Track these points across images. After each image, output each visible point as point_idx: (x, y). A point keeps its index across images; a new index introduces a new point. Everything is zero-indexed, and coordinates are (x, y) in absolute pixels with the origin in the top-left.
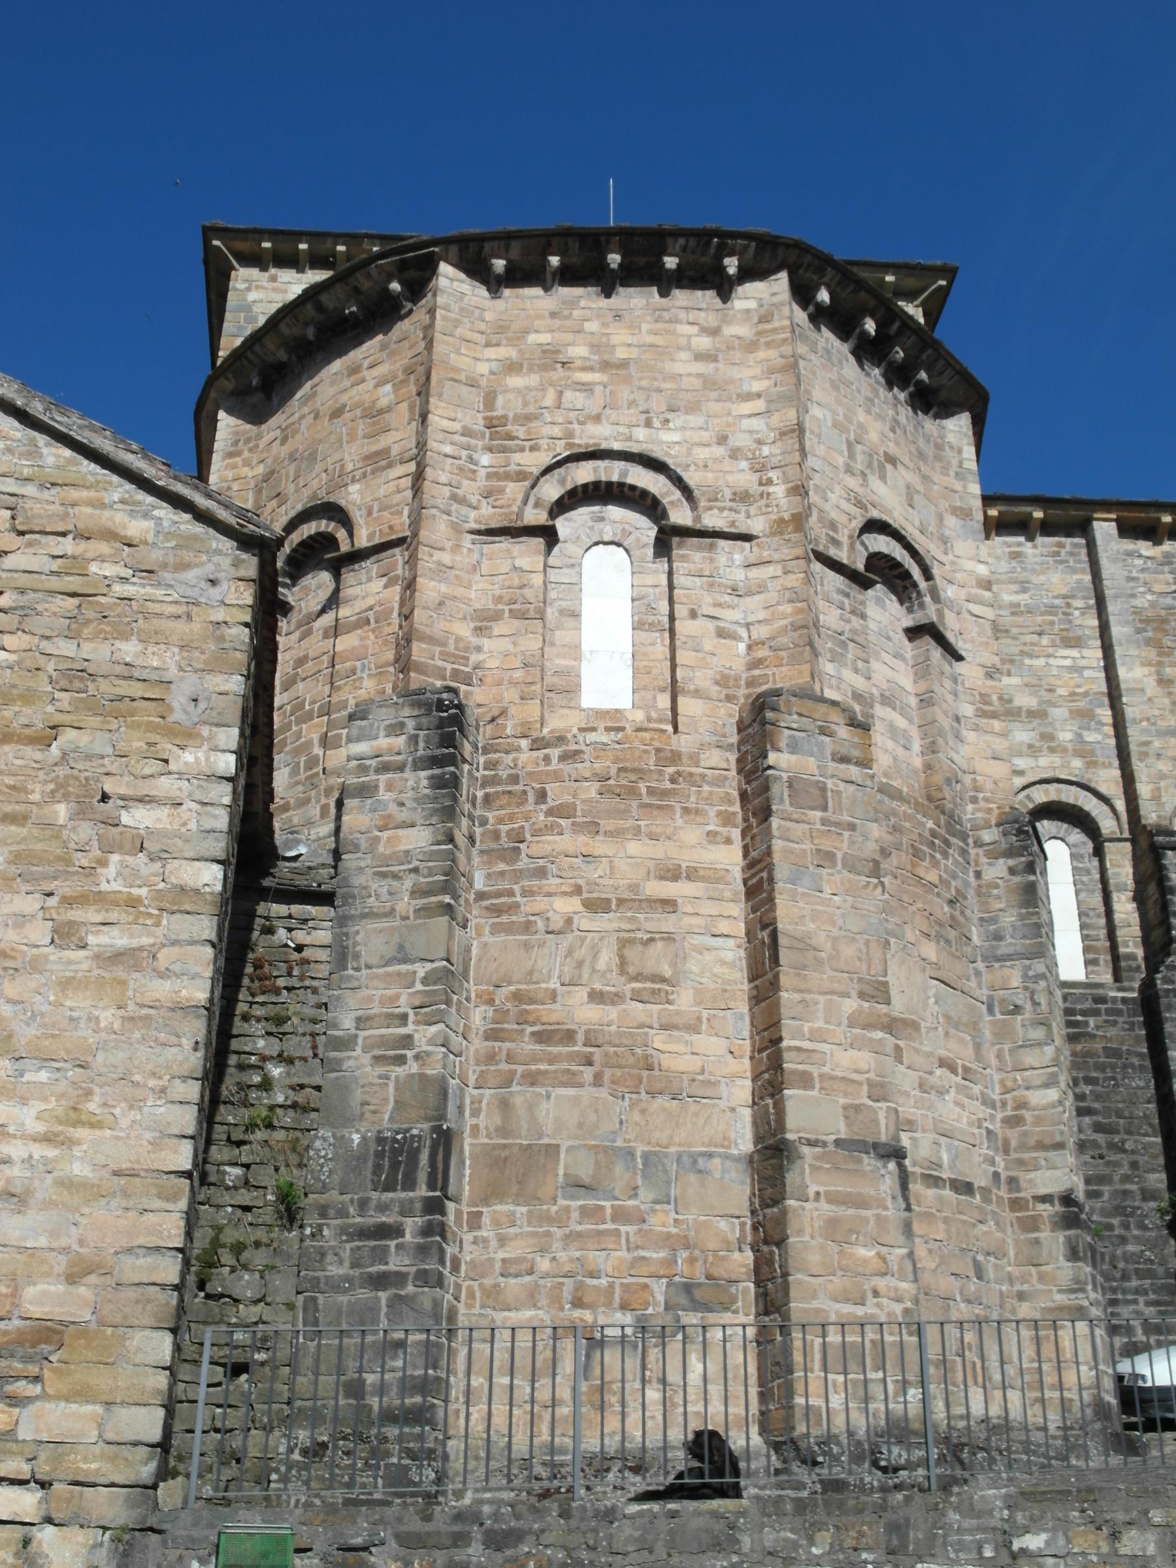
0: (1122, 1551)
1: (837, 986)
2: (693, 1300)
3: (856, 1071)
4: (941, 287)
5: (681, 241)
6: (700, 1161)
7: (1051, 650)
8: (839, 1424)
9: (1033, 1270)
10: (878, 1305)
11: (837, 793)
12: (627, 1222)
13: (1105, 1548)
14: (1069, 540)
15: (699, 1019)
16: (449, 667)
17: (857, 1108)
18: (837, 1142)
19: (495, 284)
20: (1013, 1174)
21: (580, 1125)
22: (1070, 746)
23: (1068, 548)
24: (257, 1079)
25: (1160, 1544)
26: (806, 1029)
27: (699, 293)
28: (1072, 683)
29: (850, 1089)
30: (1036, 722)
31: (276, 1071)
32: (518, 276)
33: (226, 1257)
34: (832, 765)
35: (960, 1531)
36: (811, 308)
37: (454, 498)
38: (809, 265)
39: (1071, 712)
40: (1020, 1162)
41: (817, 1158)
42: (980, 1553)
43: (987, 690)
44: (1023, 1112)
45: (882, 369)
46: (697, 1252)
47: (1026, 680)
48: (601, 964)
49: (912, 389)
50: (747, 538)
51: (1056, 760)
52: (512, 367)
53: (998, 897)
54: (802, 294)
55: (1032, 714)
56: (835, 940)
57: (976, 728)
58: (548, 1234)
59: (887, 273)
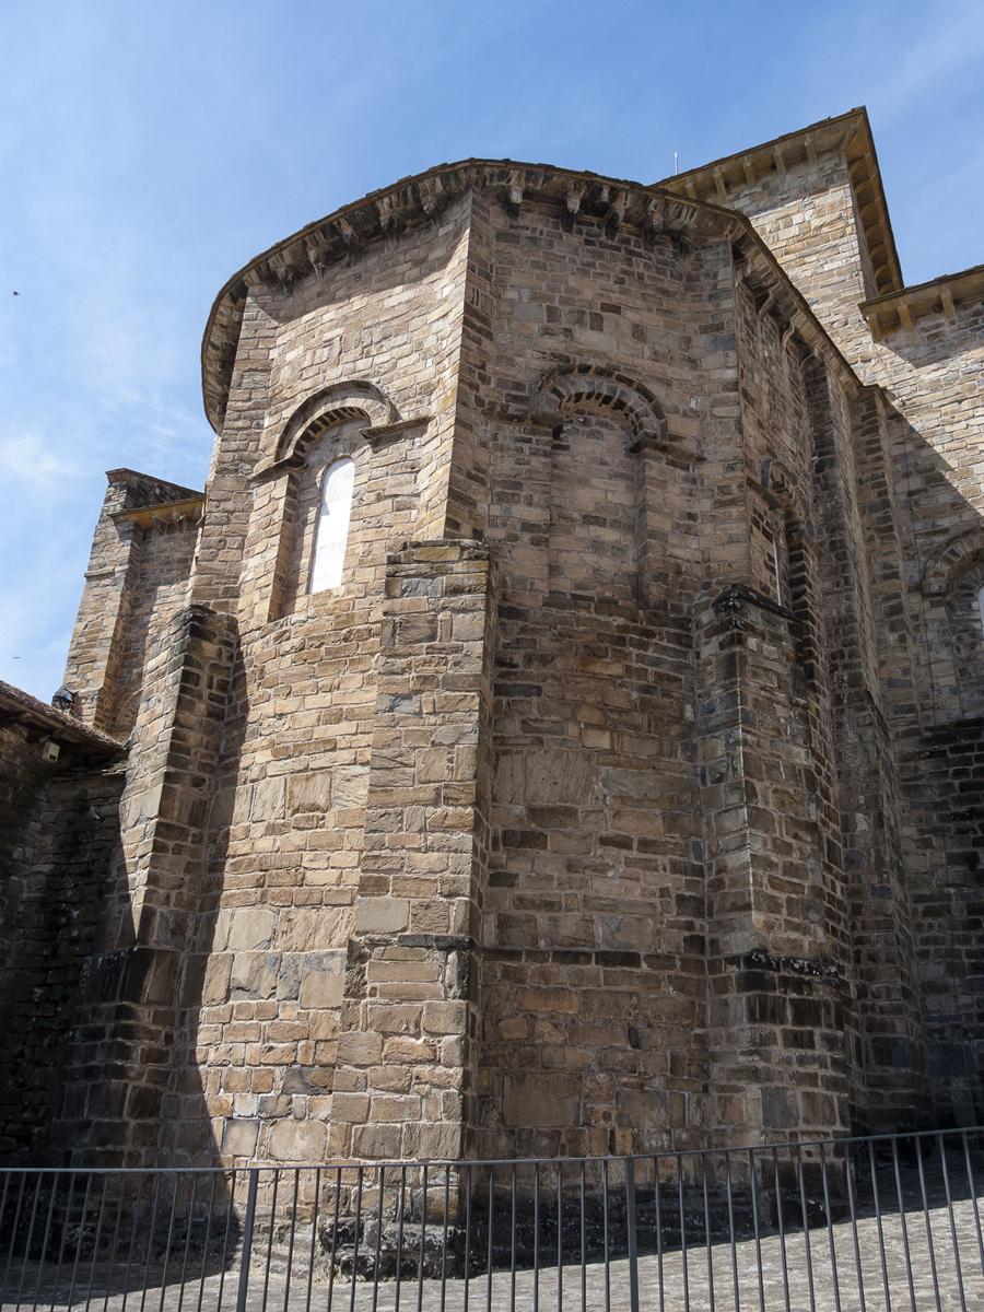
43: (727, 482)
44: (723, 875)
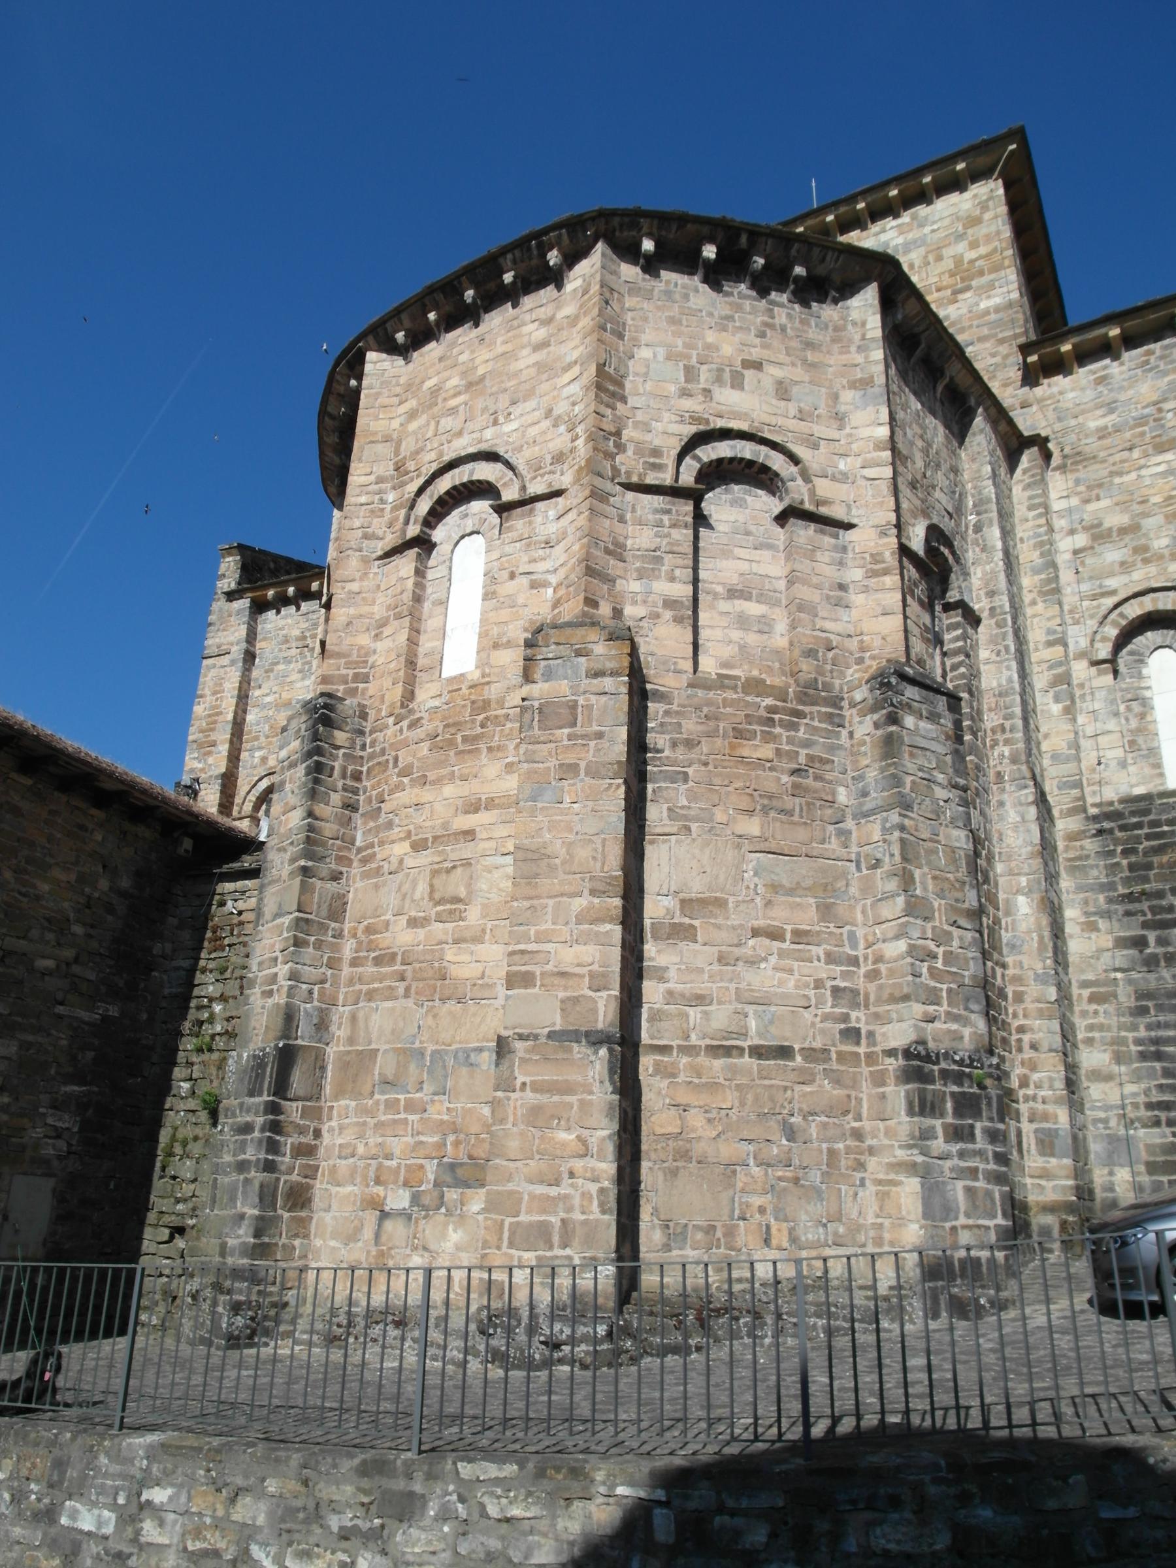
0: (235, 1517)
1: (567, 888)
2: (455, 1178)
3: (578, 965)
4: (1012, 152)
5: (509, 256)
6: (472, 1055)
7: (1142, 462)
8: (521, 1298)
9: (881, 1125)
10: (572, 1185)
11: (589, 708)
12: (413, 1112)
13: (220, 1513)
14: (1159, 344)
15: (484, 931)
16: (351, 672)
17: (576, 1000)
18: (551, 1035)
19: (403, 351)
20: (871, 1028)
21: (393, 1032)
22: (1166, 552)
23: (1158, 353)
24: (206, 1015)
25: (270, 1514)
26: (532, 933)
27: (542, 292)
28: (1167, 487)
29: (570, 983)
30: (1127, 539)
31: (218, 1008)
32: (421, 337)
33: (178, 1150)
34: (585, 682)
35: (106, 1475)
36: (642, 261)
37: (366, 537)
38: (621, 225)
39: (1167, 517)
40: (877, 1016)
41: (527, 1051)
42: (115, 1499)
45: (748, 283)
46: (462, 1136)
47: (1115, 500)
48: (417, 896)
49: (792, 287)
50: (558, 493)
51: (1152, 569)
52: (412, 415)
53: (865, 754)
54: (628, 251)
55: (1123, 531)
56: (570, 845)
57: (866, 590)
58: (365, 1124)
59: (956, 163)
